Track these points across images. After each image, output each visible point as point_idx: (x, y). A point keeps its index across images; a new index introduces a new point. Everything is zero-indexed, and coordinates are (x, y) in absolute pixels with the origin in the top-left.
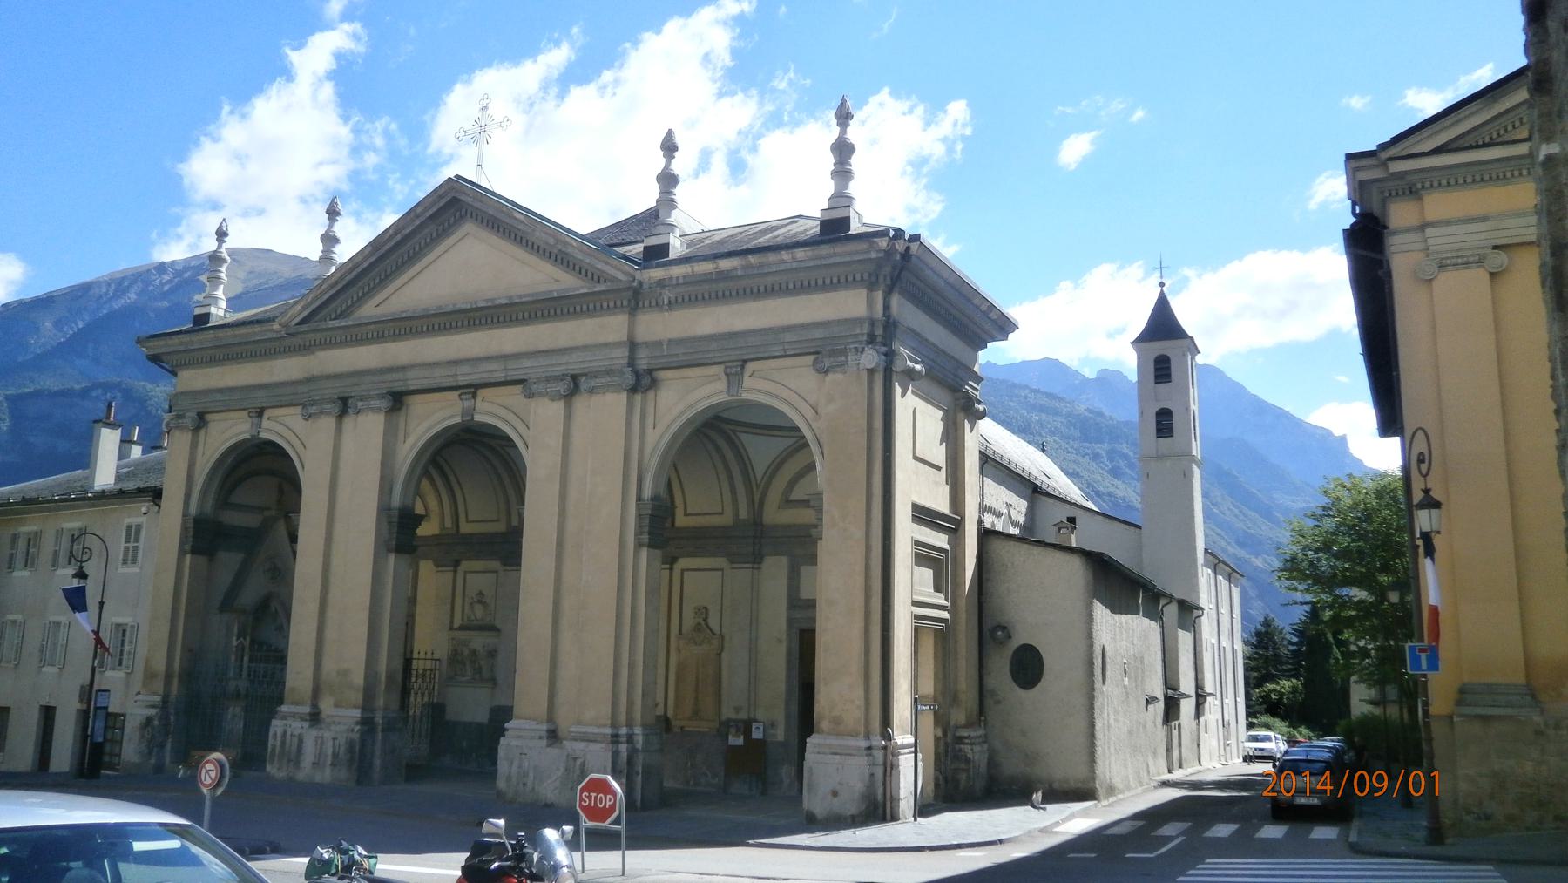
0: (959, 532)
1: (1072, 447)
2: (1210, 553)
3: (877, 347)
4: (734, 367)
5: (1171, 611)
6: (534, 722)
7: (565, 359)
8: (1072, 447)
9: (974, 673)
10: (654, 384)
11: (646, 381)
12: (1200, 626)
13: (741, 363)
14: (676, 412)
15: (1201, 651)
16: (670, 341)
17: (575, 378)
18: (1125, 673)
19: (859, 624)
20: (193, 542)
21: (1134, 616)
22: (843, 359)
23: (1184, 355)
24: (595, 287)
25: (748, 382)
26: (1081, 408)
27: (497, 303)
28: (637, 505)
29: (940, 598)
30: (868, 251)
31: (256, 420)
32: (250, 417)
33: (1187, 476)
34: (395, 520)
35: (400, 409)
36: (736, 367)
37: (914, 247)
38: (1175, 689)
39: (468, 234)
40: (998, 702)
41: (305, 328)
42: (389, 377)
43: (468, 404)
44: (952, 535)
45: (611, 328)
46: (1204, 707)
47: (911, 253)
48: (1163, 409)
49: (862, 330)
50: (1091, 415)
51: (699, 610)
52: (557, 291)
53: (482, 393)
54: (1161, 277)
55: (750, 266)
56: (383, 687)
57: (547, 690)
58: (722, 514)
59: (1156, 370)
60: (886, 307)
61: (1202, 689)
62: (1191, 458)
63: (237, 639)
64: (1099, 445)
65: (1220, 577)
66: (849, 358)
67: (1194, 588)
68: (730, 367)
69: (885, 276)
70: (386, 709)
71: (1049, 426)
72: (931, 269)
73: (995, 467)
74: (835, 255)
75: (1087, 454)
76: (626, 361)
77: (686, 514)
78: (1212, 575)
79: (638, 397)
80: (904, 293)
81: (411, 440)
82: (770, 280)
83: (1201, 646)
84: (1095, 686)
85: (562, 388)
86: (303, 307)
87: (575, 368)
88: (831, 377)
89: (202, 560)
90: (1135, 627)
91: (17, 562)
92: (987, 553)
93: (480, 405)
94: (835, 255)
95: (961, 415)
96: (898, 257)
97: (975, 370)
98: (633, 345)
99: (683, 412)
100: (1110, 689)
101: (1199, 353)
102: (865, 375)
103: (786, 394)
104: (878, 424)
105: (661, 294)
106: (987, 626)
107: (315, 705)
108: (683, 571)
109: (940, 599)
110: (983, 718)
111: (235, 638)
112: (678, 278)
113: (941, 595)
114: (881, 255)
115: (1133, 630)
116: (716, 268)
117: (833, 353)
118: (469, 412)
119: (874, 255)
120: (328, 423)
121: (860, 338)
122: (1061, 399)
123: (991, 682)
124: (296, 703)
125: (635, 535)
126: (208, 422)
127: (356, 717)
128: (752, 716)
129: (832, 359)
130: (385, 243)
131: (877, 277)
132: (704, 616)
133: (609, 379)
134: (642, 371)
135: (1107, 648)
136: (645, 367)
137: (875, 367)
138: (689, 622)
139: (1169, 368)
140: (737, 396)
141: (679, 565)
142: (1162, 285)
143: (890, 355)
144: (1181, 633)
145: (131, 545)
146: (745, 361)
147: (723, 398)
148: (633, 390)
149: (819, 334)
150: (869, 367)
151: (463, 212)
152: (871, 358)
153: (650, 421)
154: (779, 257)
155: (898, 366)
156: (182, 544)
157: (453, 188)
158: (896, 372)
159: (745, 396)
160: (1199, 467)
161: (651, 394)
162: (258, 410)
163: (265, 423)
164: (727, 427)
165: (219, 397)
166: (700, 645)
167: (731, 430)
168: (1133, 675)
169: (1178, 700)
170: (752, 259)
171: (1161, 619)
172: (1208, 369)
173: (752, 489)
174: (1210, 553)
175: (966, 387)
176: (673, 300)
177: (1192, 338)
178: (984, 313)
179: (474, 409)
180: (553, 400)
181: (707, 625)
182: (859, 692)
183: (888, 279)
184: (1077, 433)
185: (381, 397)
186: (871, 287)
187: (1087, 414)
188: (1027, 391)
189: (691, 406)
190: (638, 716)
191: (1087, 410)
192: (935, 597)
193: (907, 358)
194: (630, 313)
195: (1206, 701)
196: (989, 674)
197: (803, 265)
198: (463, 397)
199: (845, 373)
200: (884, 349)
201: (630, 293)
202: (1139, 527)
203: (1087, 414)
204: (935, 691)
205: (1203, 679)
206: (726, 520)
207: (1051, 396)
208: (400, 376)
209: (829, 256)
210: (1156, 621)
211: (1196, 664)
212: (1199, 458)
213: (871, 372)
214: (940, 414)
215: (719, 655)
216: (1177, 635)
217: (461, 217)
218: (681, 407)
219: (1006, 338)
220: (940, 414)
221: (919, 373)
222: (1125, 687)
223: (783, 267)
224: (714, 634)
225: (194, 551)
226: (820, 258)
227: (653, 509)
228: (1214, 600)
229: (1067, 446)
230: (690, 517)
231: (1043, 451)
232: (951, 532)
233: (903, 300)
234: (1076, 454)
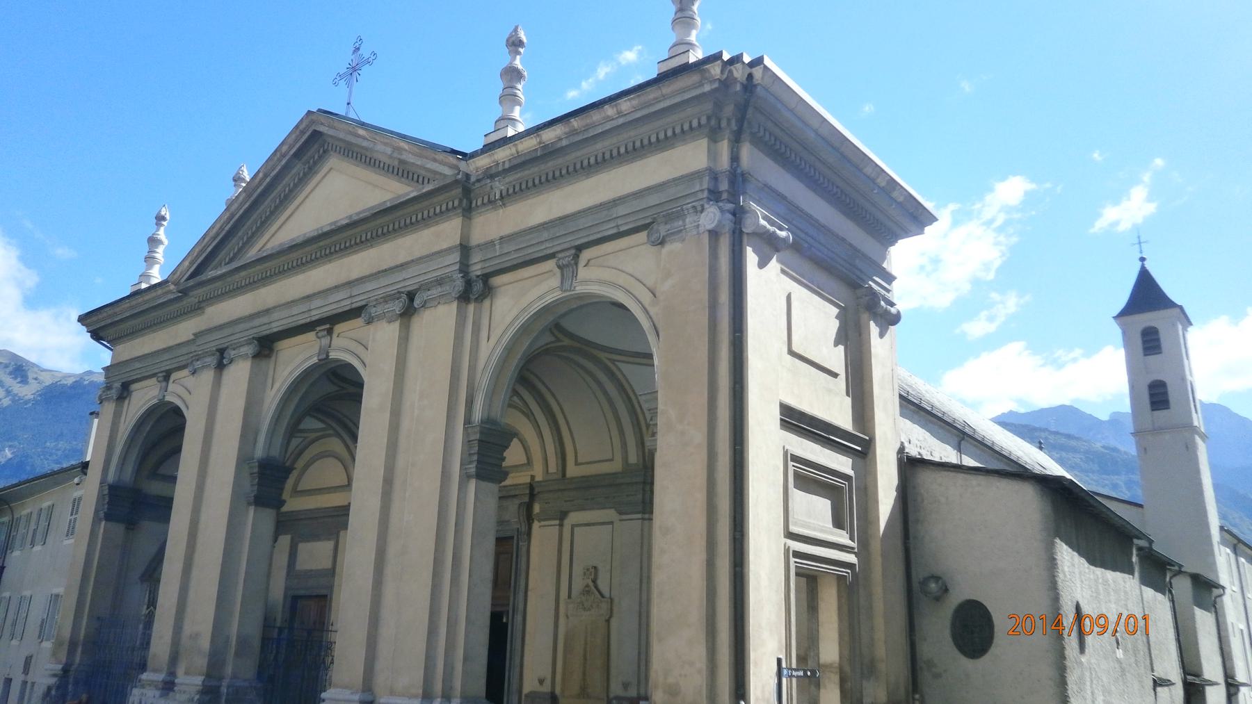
0: (870, 456)
1: (1092, 480)
2: (1226, 531)
3: (721, 204)
4: (566, 257)
5: (1183, 586)
6: (349, 692)
7: (404, 275)
8: (1092, 480)
9: (900, 640)
10: (487, 291)
11: (478, 287)
12: (1223, 608)
13: (573, 251)
14: (509, 319)
15: (1227, 637)
16: (501, 238)
17: (411, 296)
18: (1118, 643)
19: (700, 556)
20: (108, 509)
21: (1126, 576)
22: (681, 223)
23: (1174, 325)
24: (423, 188)
25: (582, 273)
26: (1098, 446)
27: (339, 224)
28: (465, 429)
29: (841, 536)
30: (701, 85)
31: (164, 384)
32: (159, 381)
33: (1190, 449)
34: (256, 470)
35: (268, 356)
36: (569, 256)
37: (757, 72)
38: (1198, 675)
39: (331, 169)
40: (937, 676)
41: (191, 283)
42: (257, 322)
43: (325, 341)
44: (859, 460)
45: (447, 233)
46: (1237, 698)
47: (755, 82)
48: (1157, 381)
49: (701, 185)
50: (1106, 451)
51: (588, 570)
52: (390, 200)
53: (339, 328)
54: (1141, 252)
55: (574, 132)
56: (233, 651)
57: (364, 652)
58: (612, 460)
59: (1144, 342)
60: (735, 159)
61: (1233, 678)
62: (1194, 430)
63: (148, 608)
64: (1116, 477)
65: (1242, 560)
66: (687, 220)
67: (1213, 566)
68: (563, 258)
69: (729, 120)
70: (234, 676)
71: (1070, 462)
72: (791, 111)
73: (975, 446)
74: (664, 97)
75: (1106, 485)
76: (457, 267)
77: (577, 464)
78: (1232, 556)
79: (471, 307)
80: (758, 142)
81: (277, 385)
82: (600, 146)
83: (1227, 630)
84: (1067, 653)
85: (397, 307)
86: (190, 263)
87: (411, 285)
88: (668, 248)
89: (119, 529)
90: (1128, 589)
91: (17, 541)
92: (914, 488)
93: (336, 342)
94: (664, 97)
95: (865, 316)
96: (738, 87)
97: (883, 265)
98: (465, 249)
99: (516, 318)
100: (1093, 661)
101: (1191, 324)
102: (706, 239)
103: (622, 280)
104: (724, 297)
105: (492, 188)
106: (919, 574)
107: (172, 674)
108: (573, 527)
109: (842, 538)
110: (917, 696)
111: (145, 607)
112: (504, 162)
113: (844, 533)
114: (716, 85)
115: (1126, 592)
116: (540, 143)
117: (670, 217)
118: (325, 351)
119: (707, 88)
120: (208, 376)
121: (700, 196)
122: (1078, 439)
123: (926, 650)
124: (155, 671)
125: (462, 465)
126: (132, 392)
127: (197, 685)
128: (642, 692)
129: (668, 227)
130: (257, 187)
131: (719, 121)
132: (593, 577)
133: (440, 289)
134: (475, 278)
135: (1082, 604)
136: (479, 273)
137: (717, 226)
138: (578, 585)
139: (1158, 340)
140: (570, 290)
141: (568, 522)
142: (1142, 259)
143: (738, 214)
144: (1199, 612)
145: (74, 517)
146: (579, 249)
147: (557, 295)
148: (464, 297)
149: (653, 200)
150: (710, 227)
151: (326, 147)
152: (711, 216)
153: (484, 334)
154: (603, 115)
155: (748, 228)
156: (96, 511)
157: (313, 122)
158: (747, 234)
159: (580, 289)
160: (1204, 441)
161: (487, 303)
162: (164, 374)
163: (171, 387)
164: (603, 356)
165: (138, 365)
166: (589, 610)
167: (609, 359)
168: (1129, 646)
169: (1203, 687)
170: (575, 123)
171: (1170, 592)
172: (1213, 410)
173: (640, 429)
174: (1226, 531)
175: (870, 283)
176: (504, 193)
177: (1181, 308)
178: (882, 189)
179: (330, 347)
180: (390, 322)
181: (596, 587)
182: (700, 651)
183: (733, 122)
184: (1096, 467)
185: (249, 343)
186: (714, 136)
187: (1103, 450)
188: (1047, 434)
189: (524, 310)
190: (458, 684)
191: (1103, 447)
192: (832, 534)
193: (761, 217)
194: (463, 216)
195: (1238, 690)
196: (925, 640)
197: (629, 118)
198: (320, 334)
199: (684, 240)
200: (730, 206)
201: (458, 191)
202: (1141, 506)
203: (1103, 450)
204: (840, 658)
205: (1233, 668)
206: (616, 466)
207: (1069, 436)
208: (265, 320)
209: (657, 100)
210: (1164, 594)
211: (1221, 649)
212: (1203, 430)
213: (714, 234)
214: (835, 311)
215: (608, 621)
216: (1194, 614)
217: (325, 152)
218: (515, 312)
219: (921, 232)
220: (835, 311)
221: (785, 240)
222: (1118, 661)
223: (608, 126)
224: (602, 596)
225: (109, 517)
226: (648, 105)
227: (481, 433)
228: (1237, 582)
229: (1087, 478)
230: (582, 467)
231: (1041, 448)
232: (856, 455)
233: (756, 151)
234: (1096, 485)
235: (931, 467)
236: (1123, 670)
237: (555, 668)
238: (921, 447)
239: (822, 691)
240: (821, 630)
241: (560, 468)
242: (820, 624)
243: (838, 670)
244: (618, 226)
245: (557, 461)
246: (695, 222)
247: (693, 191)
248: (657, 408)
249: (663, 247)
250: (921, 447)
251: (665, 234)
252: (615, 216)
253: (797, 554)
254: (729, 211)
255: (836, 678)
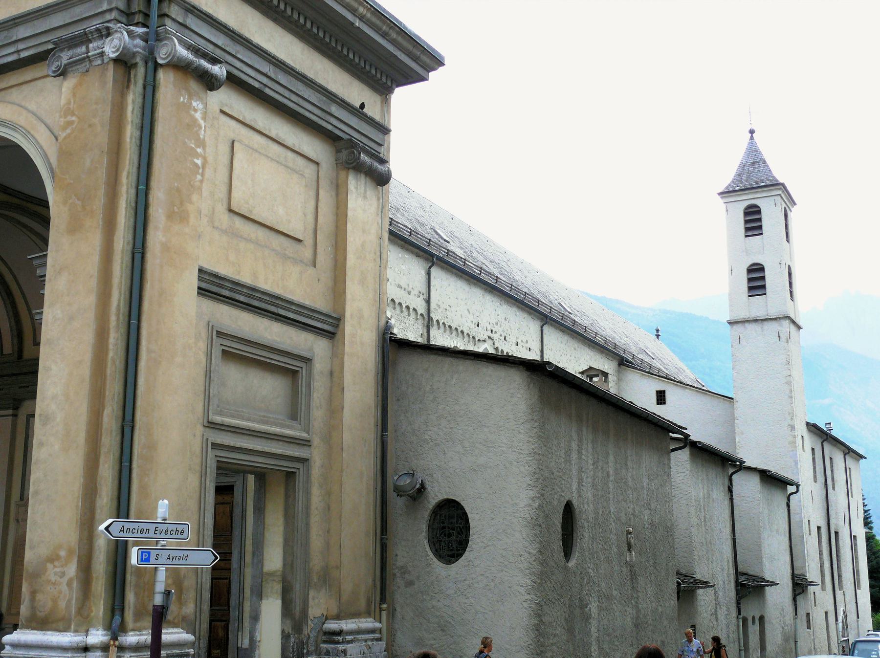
110: (384, 606)
129: (70, 53)
177: (783, 185)
192: (288, 427)
204: (284, 565)
213: (124, 63)
235: (418, 350)
236: (633, 576)
237: (115, 581)
238: (492, 331)
239: (264, 601)
240: (267, 534)
241: (16, 348)
242: (266, 526)
243: (281, 579)
244: (18, 52)
245: (12, 340)
246: (99, 48)
247: (100, 10)
248: (45, 276)
249: (65, 79)
250: (492, 331)
251: (66, 62)
252: (14, 38)
253: (215, 446)
254: (140, 37)
255: (278, 587)
